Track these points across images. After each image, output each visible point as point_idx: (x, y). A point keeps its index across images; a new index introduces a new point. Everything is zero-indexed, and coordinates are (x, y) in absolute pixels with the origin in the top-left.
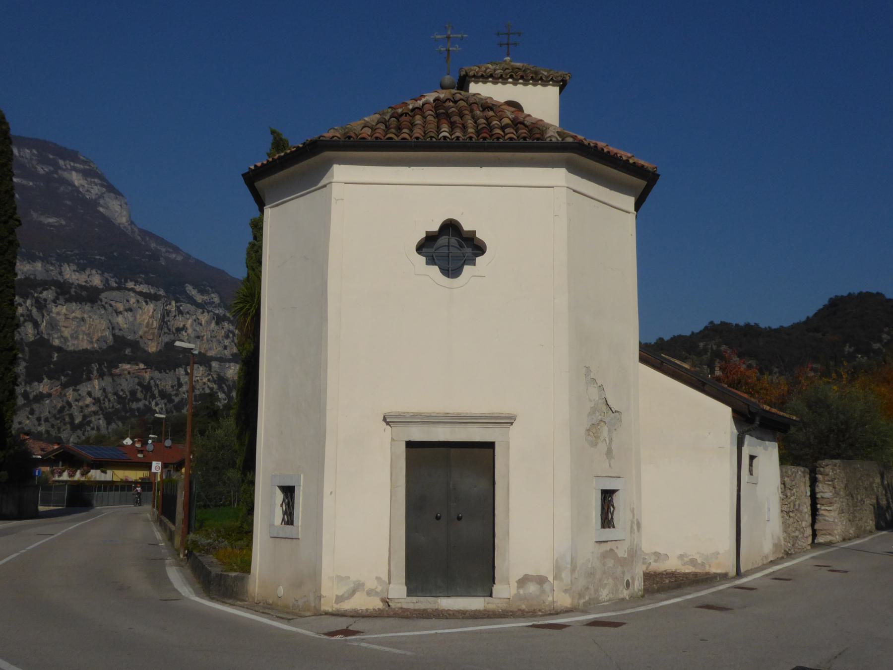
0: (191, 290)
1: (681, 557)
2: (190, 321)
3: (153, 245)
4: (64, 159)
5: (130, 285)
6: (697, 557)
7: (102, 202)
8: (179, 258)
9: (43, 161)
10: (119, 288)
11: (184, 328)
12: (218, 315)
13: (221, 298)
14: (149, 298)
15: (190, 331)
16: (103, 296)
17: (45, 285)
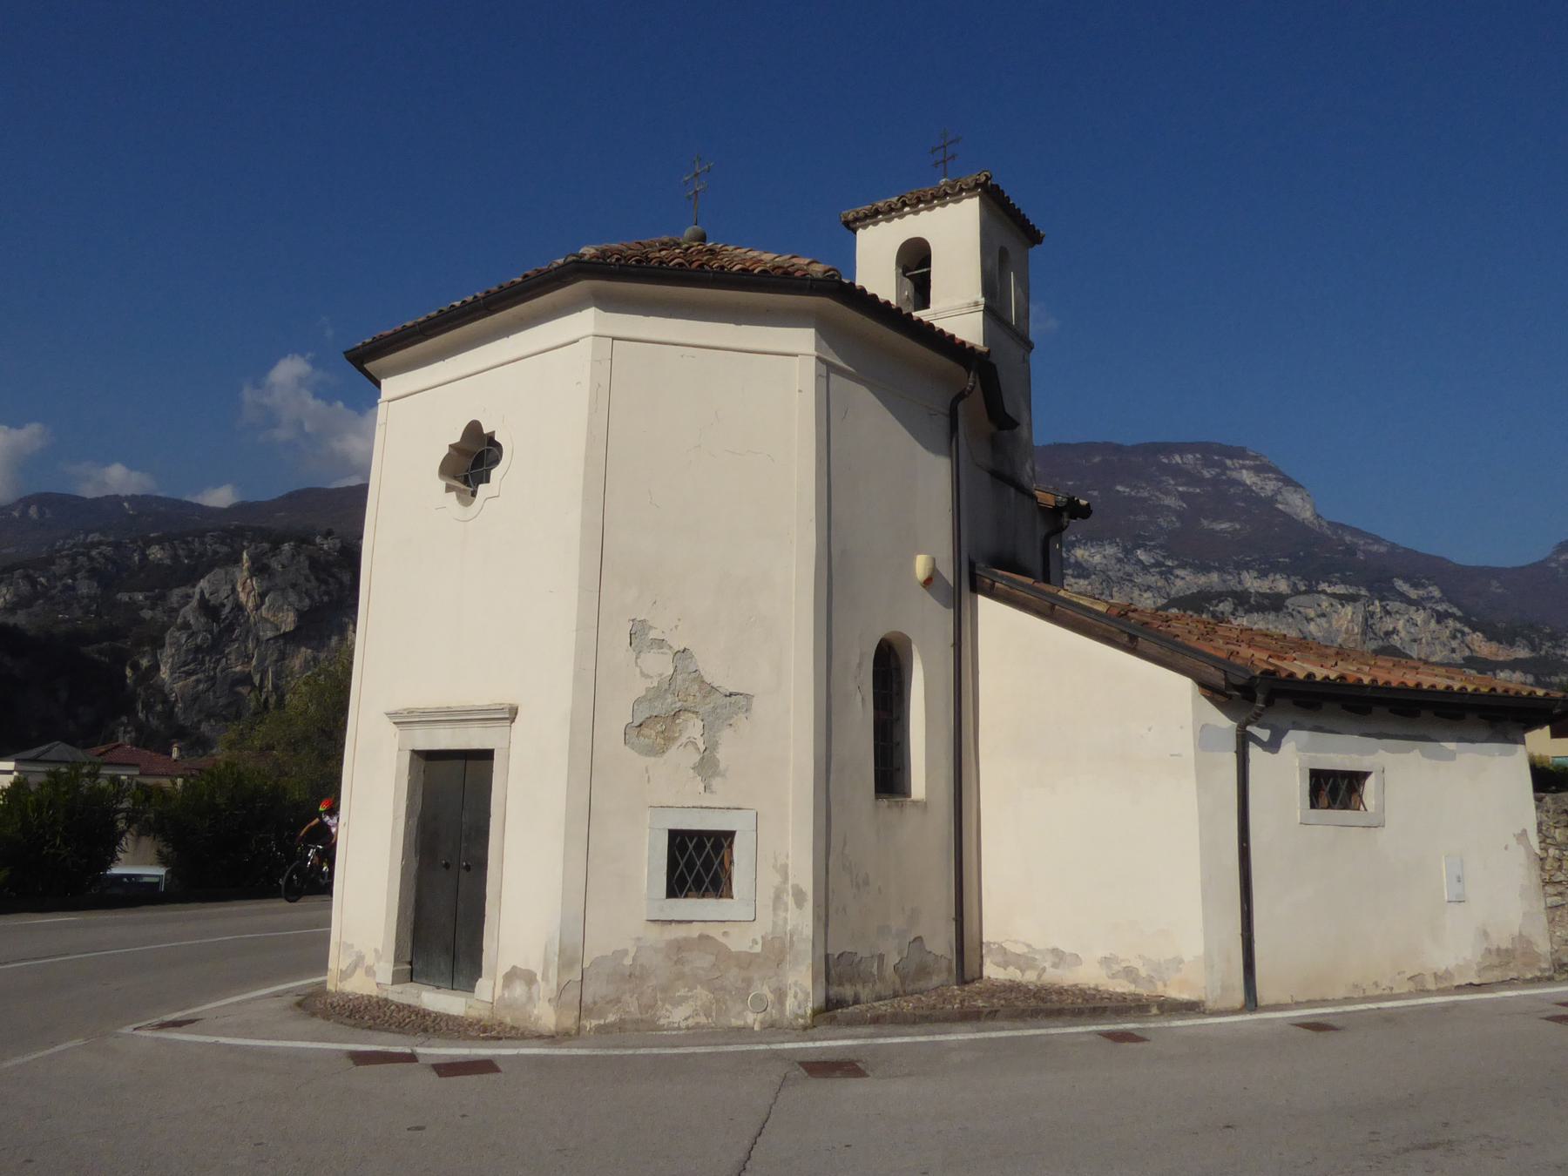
0: (1400, 585)
1: (1106, 961)
2: (1401, 623)
3: (1348, 539)
4: (1231, 458)
5: (1324, 586)
6: (1137, 964)
7: (1279, 498)
8: (1383, 549)
9: (1208, 464)
10: (1310, 591)
11: (1395, 631)
12: (1438, 612)
13: (1442, 591)
14: (1344, 599)
15: (1403, 634)
16: (1288, 602)
17: (1220, 597)
